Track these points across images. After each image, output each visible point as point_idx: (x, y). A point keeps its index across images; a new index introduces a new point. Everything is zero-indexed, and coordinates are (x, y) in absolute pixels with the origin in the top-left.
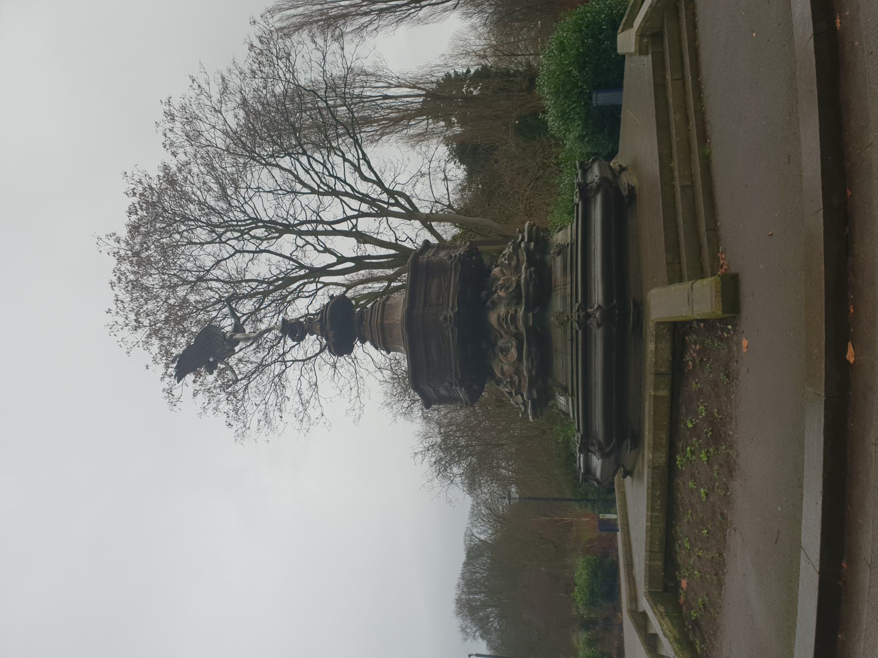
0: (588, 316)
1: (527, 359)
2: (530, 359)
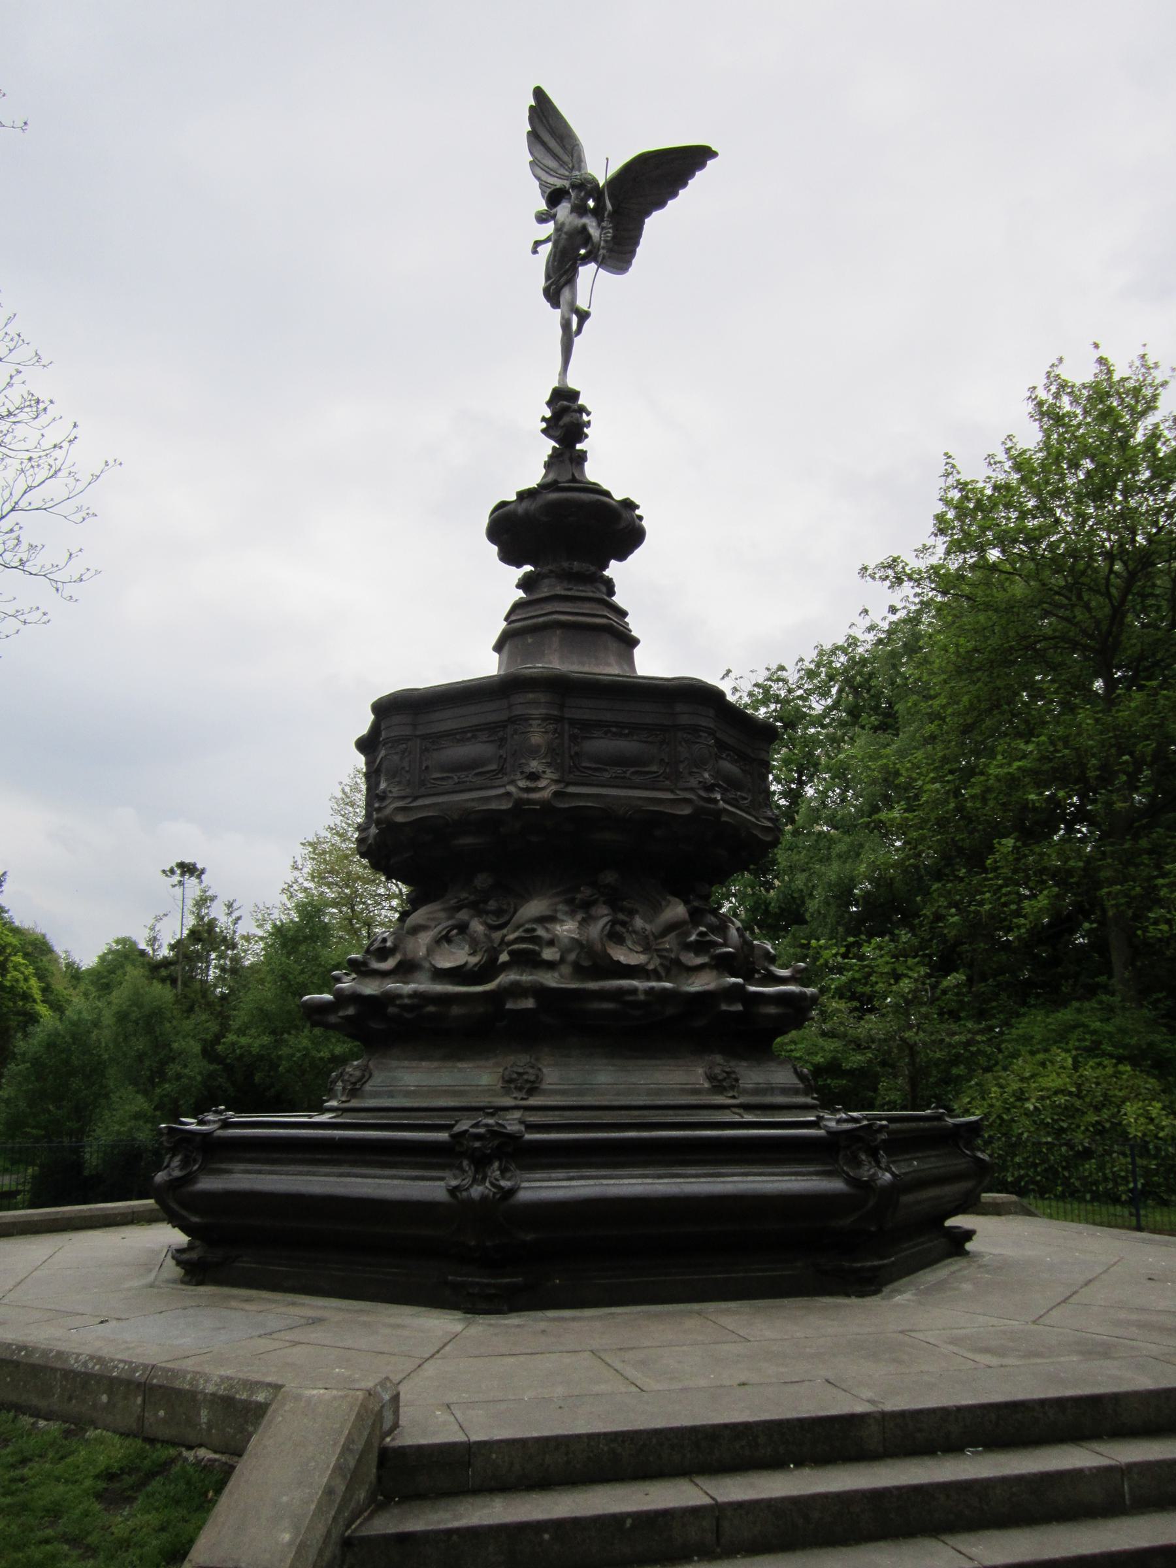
0: (481, 1162)
2: (416, 1001)
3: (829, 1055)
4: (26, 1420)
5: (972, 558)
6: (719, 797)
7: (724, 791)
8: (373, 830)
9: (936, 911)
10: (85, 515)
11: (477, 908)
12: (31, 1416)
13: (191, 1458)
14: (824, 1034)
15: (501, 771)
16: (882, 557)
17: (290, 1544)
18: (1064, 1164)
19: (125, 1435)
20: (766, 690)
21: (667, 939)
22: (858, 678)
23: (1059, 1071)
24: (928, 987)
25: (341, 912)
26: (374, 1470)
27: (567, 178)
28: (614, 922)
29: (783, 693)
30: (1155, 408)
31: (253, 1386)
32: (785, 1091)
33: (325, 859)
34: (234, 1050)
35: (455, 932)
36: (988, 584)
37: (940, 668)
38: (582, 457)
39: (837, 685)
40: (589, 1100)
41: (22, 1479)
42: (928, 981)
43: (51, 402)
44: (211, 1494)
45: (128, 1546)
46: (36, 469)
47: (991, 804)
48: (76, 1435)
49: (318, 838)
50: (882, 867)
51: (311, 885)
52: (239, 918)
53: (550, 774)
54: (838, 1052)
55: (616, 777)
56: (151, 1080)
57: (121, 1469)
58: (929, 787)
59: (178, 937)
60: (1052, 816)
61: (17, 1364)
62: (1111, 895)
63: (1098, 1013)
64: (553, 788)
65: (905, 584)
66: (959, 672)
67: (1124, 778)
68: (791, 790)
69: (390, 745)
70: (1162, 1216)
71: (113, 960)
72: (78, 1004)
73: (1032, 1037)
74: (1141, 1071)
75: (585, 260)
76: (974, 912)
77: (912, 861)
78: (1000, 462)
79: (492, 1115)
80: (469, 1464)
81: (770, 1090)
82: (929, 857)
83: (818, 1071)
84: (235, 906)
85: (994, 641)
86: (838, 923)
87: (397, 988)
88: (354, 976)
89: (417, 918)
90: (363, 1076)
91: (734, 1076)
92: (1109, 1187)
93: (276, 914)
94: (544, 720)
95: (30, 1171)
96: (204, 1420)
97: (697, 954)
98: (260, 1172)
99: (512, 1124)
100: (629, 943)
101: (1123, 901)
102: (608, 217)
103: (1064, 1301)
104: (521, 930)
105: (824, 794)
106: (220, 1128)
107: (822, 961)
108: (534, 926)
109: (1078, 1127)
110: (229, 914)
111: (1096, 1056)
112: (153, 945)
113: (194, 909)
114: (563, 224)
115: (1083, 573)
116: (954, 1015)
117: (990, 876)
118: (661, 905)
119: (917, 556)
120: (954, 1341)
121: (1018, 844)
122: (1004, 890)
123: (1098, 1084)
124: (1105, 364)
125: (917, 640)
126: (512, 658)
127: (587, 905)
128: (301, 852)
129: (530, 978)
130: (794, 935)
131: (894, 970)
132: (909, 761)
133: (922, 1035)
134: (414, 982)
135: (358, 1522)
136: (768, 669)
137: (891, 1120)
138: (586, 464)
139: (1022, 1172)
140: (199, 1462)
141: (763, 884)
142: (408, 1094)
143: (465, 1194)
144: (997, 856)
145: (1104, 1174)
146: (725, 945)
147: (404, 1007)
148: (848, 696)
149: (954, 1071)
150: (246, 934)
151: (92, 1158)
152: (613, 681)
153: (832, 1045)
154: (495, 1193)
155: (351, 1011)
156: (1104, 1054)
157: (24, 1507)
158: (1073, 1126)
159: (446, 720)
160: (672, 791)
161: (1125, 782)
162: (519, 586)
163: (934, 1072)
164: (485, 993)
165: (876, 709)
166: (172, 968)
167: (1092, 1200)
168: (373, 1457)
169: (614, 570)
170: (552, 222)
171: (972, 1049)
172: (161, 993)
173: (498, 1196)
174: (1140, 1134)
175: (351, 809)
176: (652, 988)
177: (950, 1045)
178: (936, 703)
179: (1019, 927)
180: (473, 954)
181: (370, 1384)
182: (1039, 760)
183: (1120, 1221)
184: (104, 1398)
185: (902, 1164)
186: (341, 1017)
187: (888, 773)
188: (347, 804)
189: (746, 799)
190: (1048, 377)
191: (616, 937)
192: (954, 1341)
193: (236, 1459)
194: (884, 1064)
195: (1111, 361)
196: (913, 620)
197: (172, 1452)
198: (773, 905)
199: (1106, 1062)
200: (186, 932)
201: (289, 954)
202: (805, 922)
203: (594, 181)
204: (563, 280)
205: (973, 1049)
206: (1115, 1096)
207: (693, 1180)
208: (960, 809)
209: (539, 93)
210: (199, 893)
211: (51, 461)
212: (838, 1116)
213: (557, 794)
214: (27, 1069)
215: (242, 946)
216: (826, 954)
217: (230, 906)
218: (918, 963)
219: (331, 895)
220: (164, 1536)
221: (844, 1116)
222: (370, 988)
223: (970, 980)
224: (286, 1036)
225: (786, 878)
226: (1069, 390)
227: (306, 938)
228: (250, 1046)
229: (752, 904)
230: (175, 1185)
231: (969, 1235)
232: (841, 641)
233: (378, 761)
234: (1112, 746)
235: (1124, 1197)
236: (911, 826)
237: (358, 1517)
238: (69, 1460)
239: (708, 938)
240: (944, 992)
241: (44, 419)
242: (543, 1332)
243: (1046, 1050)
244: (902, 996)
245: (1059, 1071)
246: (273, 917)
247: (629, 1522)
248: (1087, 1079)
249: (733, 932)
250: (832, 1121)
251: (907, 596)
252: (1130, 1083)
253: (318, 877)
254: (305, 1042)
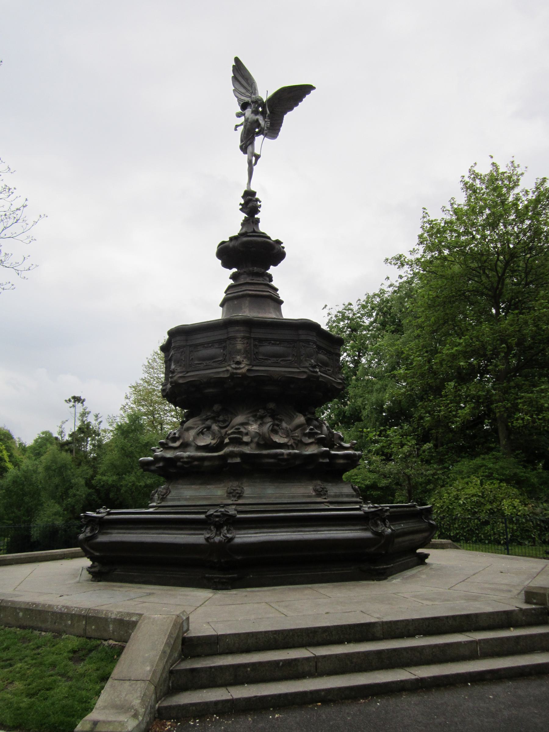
0: (219, 527)
1: (289, 454)
2: (189, 460)
3: (372, 481)
4: (37, 633)
5: (436, 254)
6: (318, 370)
7: (320, 367)
8: (169, 386)
9: (420, 415)
10: (31, 240)
11: (215, 419)
12: (39, 631)
13: (106, 644)
14: (370, 471)
15: (225, 360)
16: (395, 254)
17: (150, 671)
18: (476, 527)
19: (79, 636)
20: (343, 315)
21: (297, 431)
22: (385, 309)
23: (474, 486)
24: (416, 449)
25: (148, 418)
26: (180, 646)
27: (250, 97)
28: (273, 425)
29: (351, 316)
30: (518, 185)
31: (130, 614)
32: (348, 496)
33: (140, 394)
34: (100, 483)
35: (205, 430)
36: (443, 266)
37: (421, 305)
38: (258, 221)
39: (375, 312)
40: (264, 501)
41: (39, 654)
42: (416, 447)
43: (15, 189)
44: (115, 657)
45: (85, 676)
46: (8, 220)
47: (444, 366)
48: (58, 637)
49: (137, 384)
50: (396, 395)
51: (134, 406)
52: (101, 422)
53: (246, 362)
54: (376, 479)
55: (274, 362)
56: (61, 497)
57: (79, 649)
58: (416, 359)
59: (73, 430)
60: (472, 371)
61: (32, 610)
62: (498, 408)
63: (492, 460)
64: (247, 368)
65: (405, 266)
66: (429, 307)
67: (503, 354)
68: (355, 360)
69: (176, 349)
70: (518, 549)
71: (41, 442)
72: (26, 463)
73: (463, 471)
74: (511, 486)
75: (258, 134)
76: (436, 415)
77: (409, 392)
78: (448, 210)
79: (223, 507)
80: (218, 643)
81: (341, 495)
82: (417, 390)
83: (368, 487)
84: (99, 416)
85: (445, 293)
86: (376, 421)
87: (181, 454)
88: (162, 449)
89: (188, 424)
90: (167, 492)
91: (325, 490)
92: (496, 537)
93: (118, 420)
94: (242, 338)
95: (6, 540)
96: (111, 629)
97: (309, 438)
98: (124, 533)
99: (232, 511)
100: (280, 434)
101: (503, 409)
102: (268, 116)
103: (463, 581)
104: (234, 428)
105: (370, 362)
106: (107, 515)
107: (369, 438)
108: (239, 427)
109: (483, 511)
110: (96, 420)
111: (491, 479)
112: (61, 435)
113: (80, 418)
114: (248, 118)
115: (485, 261)
116: (428, 462)
117: (444, 399)
118: (294, 417)
119: (411, 254)
120: (414, 596)
121: (456, 385)
122: (450, 406)
123: (491, 492)
124: (495, 166)
125: (411, 292)
126: (228, 309)
127: (262, 418)
128: (129, 391)
129: (238, 449)
130: (356, 426)
131: (401, 441)
132: (408, 347)
133: (413, 471)
134: (189, 452)
135: (175, 665)
136: (344, 305)
137: (391, 507)
138: (259, 224)
139: (458, 531)
140: (109, 645)
141: (342, 403)
142: (186, 499)
143: (212, 540)
144: (447, 390)
145: (494, 532)
146: (321, 434)
147: (184, 463)
148: (380, 317)
149: (428, 487)
150: (104, 429)
151: (35, 533)
152: (272, 321)
153: (373, 476)
154: (225, 540)
155: (161, 464)
156: (494, 479)
157: (41, 664)
158: (480, 511)
159: (200, 339)
160: (298, 368)
161: (504, 356)
162: (230, 278)
163: (420, 488)
164: (219, 456)
165: (393, 322)
166: (71, 445)
167: (489, 543)
168: (180, 641)
169: (272, 270)
170: (243, 117)
171: (435, 477)
172: (66, 457)
173: (226, 541)
174: (509, 514)
175: (152, 370)
176: (290, 453)
177: (426, 475)
178: (420, 320)
179: (456, 422)
180: (213, 439)
181: (178, 613)
182: (465, 347)
183: (500, 551)
184: (69, 622)
185: (397, 525)
186: (156, 467)
187: (399, 352)
188: (150, 368)
189: (330, 370)
190: (470, 172)
191: (274, 431)
192: (414, 596)
193: (124, 643)
194: (397, 484)
195: (498, 164)
196: (410, 282)
197: (99, 642)
198: (347, 413)
199: (495, 482)
200: (77, 428)
201: (125, 438)
202: (362, 420)
203: (261, 100)
204: (249, 142)
205: (436, 477)
206: (499, 497)
207: (308, 533)
208: (431, 367)
209: (237, 60)
210: (82, 410)
211: (15, 216)
212: (369, 506)
213: (249, 370)
214: (4, 493)
215: (103, 434)
216: (371, 435)
217: (97, 416)
218: (412, 438)
219: (143, 410)
220: (99, 672)
221: (371, 505)
222: (169, 454)
223: (436, 446)
224: (124, 476)
225: (353, 401)
226: (479, 177)
227: (132, 431)
228: (107, 480)
229: (337, 412)
230: (88, 539)
231: (427, 556)
232: (377, 292)
233: (170, 356)
234: (498, 340)
235: (502, 542)
236: (409, 376)
237: (175, 663)
238: (57, 646)
239: (314, 431)
240: (424, 451)
241: (12, 197)
242: (246, 596)
243: (469, 477)
244: (404, 454)
245: (474, 486)
246: (116, 421)
247: (281, 663)
248: (487, 490)
249: (325, 428)
250: (366, 508)
251: (406, 272)
252: (506, 491)
253: (137, 402)
254: (133, 479)
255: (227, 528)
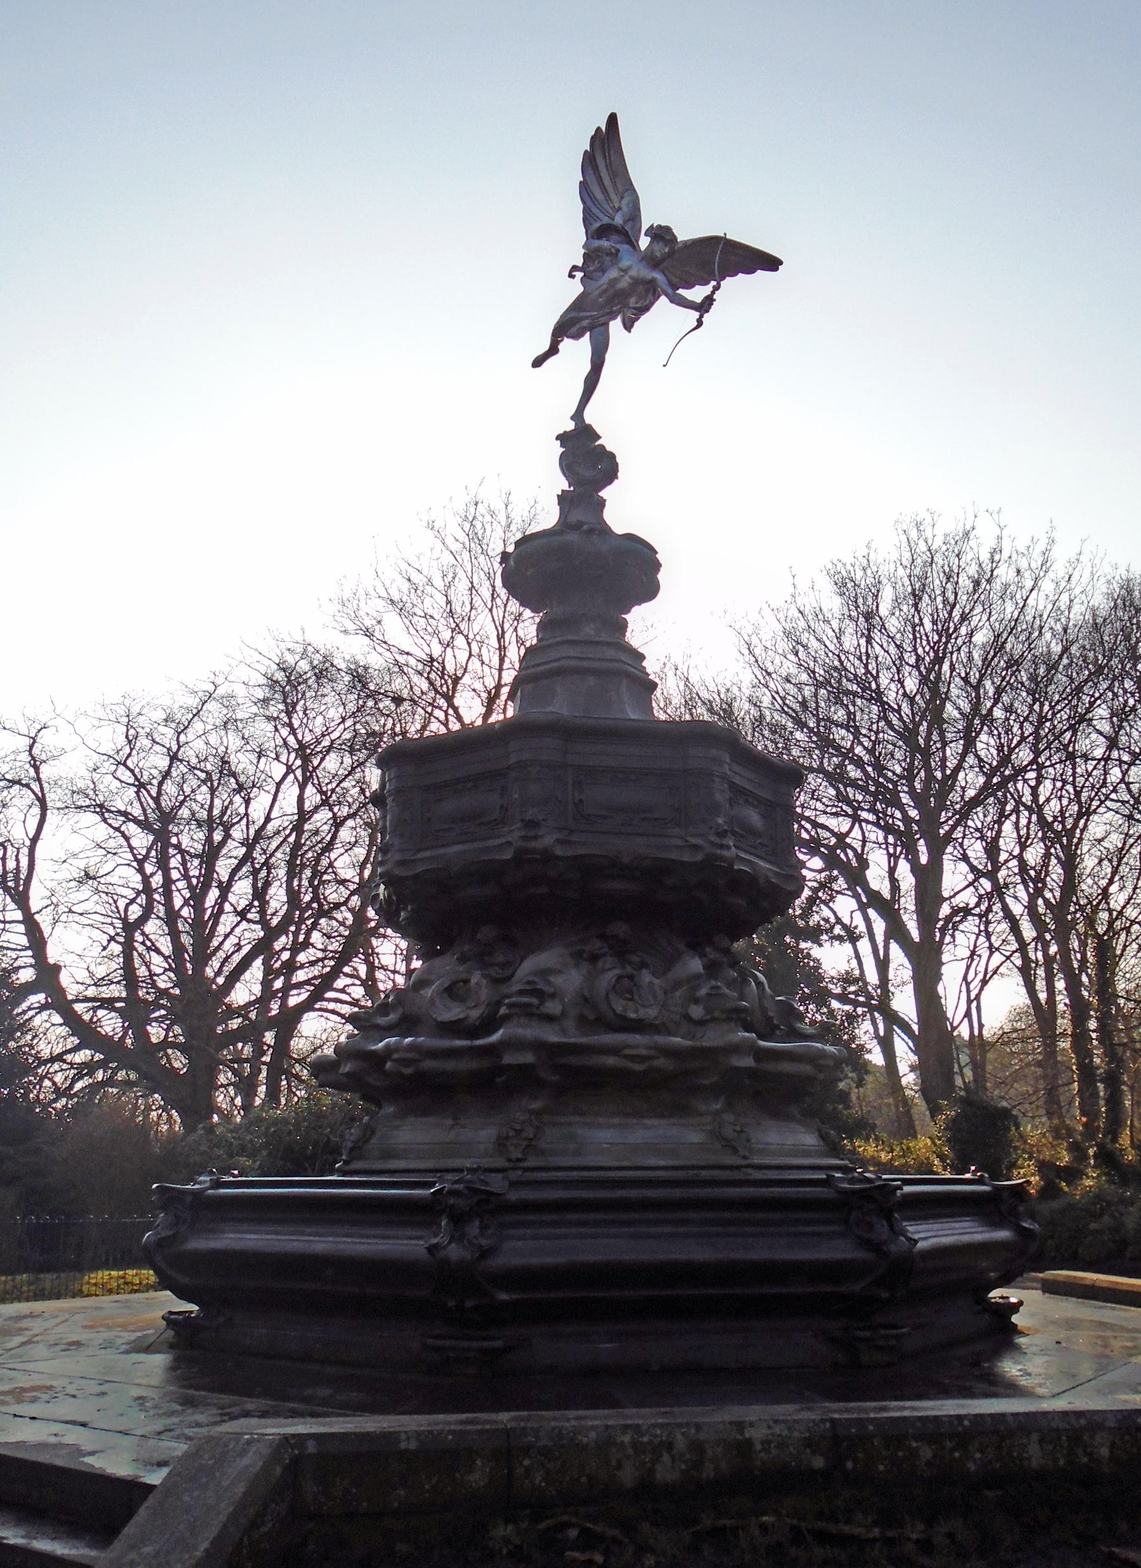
32: (806, 1154)
99: (496, 1183)
127: (594, 958)
147: (403, 1062)
255: (481, 1222)
